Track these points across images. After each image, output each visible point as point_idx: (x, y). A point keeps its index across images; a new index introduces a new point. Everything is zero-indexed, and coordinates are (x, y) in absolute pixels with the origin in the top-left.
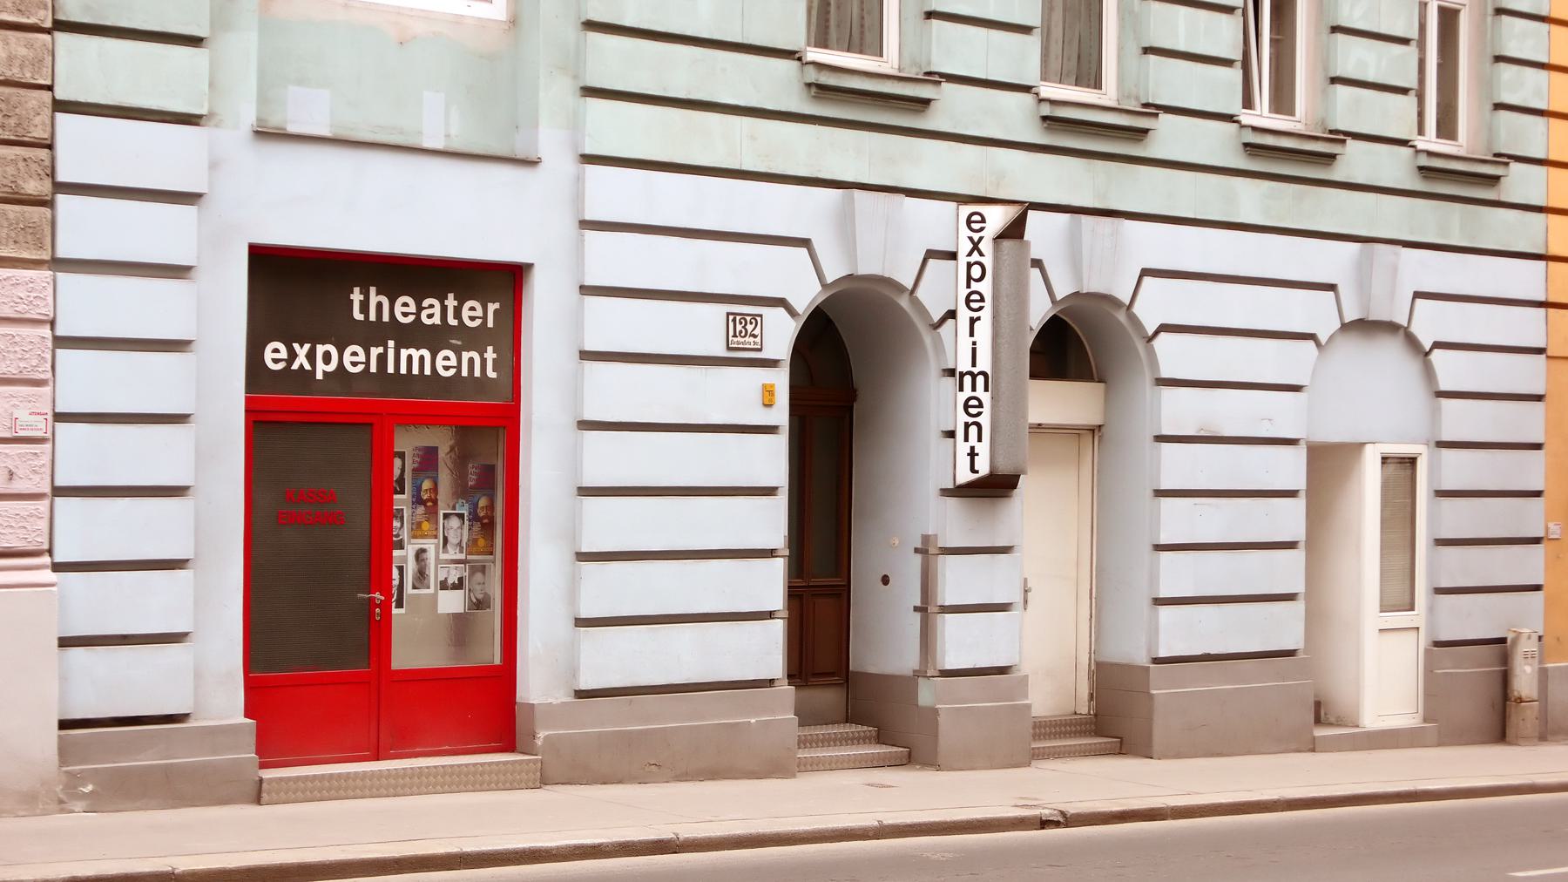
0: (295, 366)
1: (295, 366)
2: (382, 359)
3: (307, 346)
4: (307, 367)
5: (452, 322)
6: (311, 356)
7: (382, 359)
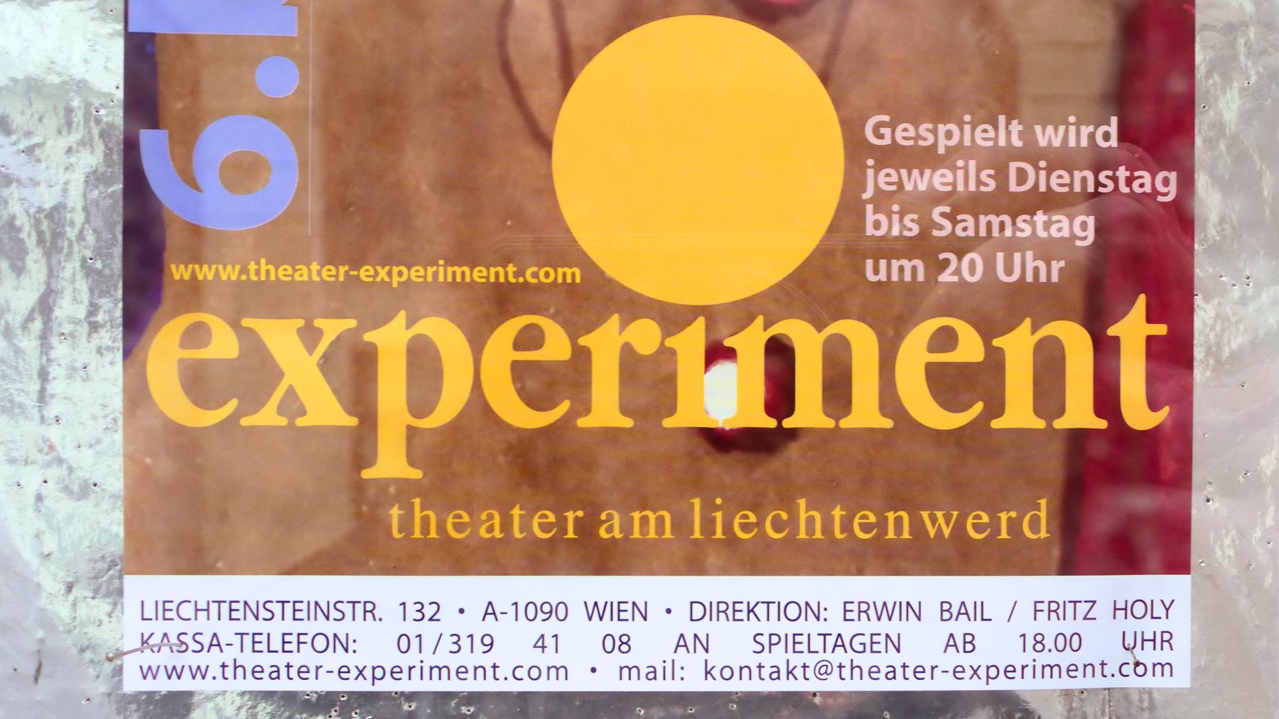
0: (378, 279)
1: (378, 279)
2: (435, 274)
3: (387, 268)
4: (387, 279)
5: (1124, 189)
6: (390, 274)
7: (435, 274)
